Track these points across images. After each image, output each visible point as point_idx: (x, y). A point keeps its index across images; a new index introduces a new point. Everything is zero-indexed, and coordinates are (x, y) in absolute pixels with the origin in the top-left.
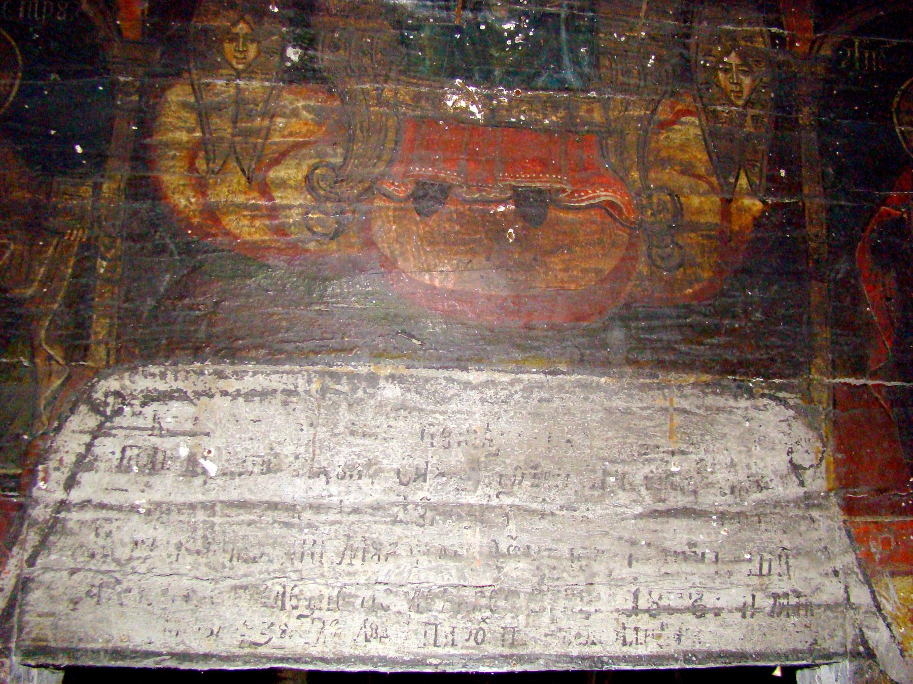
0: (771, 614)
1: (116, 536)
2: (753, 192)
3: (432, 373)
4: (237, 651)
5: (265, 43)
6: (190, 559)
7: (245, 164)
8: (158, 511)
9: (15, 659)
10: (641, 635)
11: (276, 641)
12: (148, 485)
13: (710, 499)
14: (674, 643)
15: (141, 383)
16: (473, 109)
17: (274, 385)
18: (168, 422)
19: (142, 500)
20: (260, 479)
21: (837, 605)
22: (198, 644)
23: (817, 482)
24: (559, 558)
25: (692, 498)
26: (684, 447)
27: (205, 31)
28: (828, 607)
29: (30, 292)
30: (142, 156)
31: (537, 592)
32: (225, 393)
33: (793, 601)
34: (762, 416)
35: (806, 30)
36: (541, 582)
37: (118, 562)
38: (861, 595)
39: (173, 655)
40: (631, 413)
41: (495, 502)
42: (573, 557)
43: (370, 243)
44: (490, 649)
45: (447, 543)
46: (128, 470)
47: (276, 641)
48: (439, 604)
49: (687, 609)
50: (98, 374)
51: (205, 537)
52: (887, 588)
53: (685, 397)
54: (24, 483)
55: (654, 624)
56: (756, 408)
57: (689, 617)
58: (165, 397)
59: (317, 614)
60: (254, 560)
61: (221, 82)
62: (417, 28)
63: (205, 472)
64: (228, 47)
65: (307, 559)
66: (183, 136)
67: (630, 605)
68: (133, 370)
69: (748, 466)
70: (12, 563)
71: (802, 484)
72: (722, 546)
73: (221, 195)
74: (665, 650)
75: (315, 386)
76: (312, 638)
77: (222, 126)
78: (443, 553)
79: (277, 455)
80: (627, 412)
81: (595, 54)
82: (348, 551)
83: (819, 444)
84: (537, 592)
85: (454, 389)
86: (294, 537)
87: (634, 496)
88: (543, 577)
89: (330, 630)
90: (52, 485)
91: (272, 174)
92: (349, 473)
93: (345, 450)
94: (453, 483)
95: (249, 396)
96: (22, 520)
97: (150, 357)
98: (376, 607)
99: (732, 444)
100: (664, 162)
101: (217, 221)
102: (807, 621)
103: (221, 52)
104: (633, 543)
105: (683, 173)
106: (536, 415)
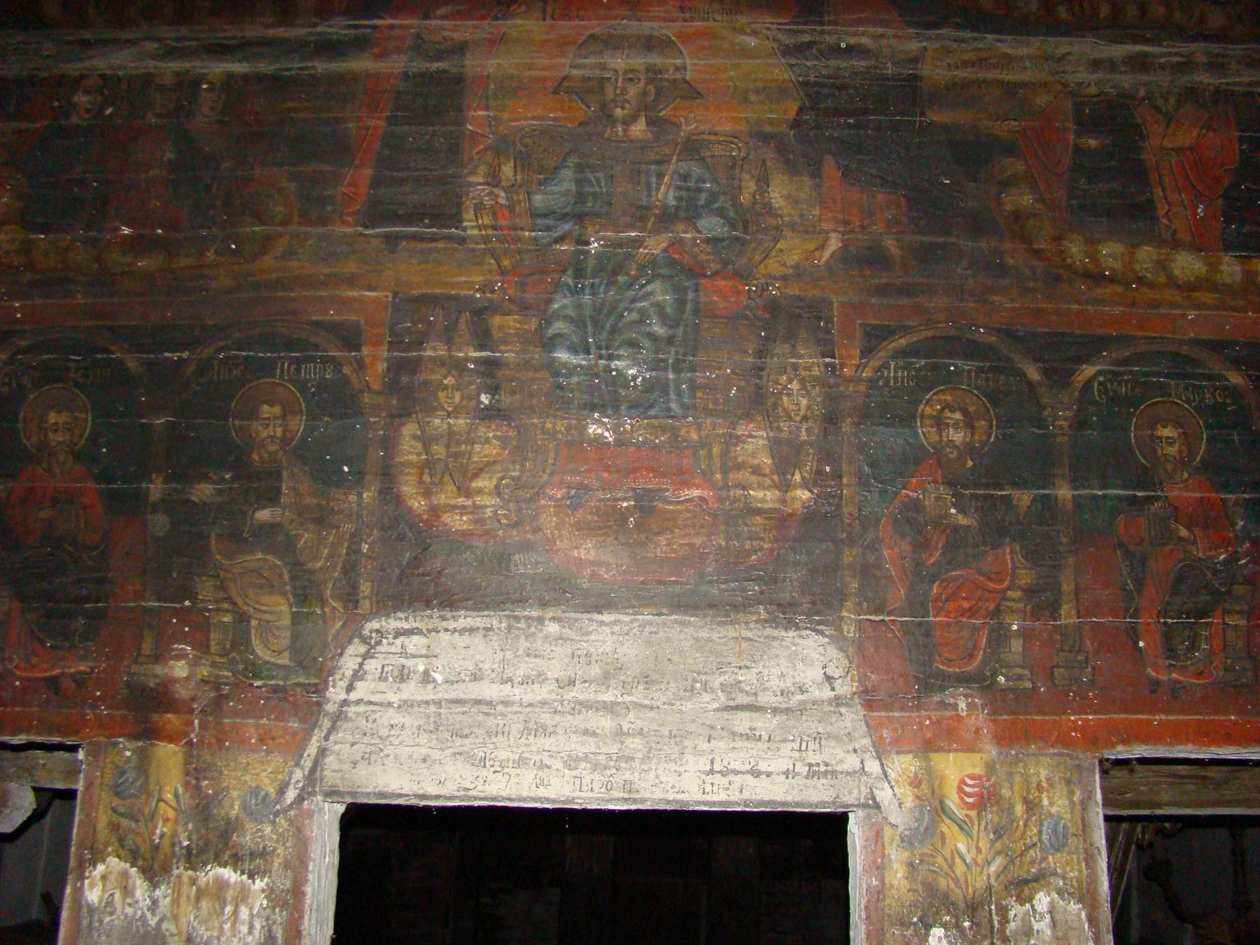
0: (807, 777)
1: (379, 721)
2: (805, 485)
3: (579, 615)
4: (457, 794)
5: (465, 391)
6: (426, 736)
7: (456, 477)
8: (405, 705)
9: (320, 798)
10: (715, 788)
11: (480, 787)
12: (398, 689)
13: (765, 699)
14: (737, 794)
15: (393, 624)
16: (607, 434)
17: (478, 624)
18: (411, 649)
19: (395, 699)
20: (471, 685)
21: (855, 772)
22: (433, 790)
23: (845, 688)
24: (662, 737)
25: (753, 698)
26: (748, 664)
27: (426, 383)
28: (848, 773)
29: (319, 565)
30: (388, 475)
31: (646, 758)
32: (446, 630)
33: (823, 768)
34: (804, 642)
35: (851, 357)
36: (649, 752)
37: (381, 738)
38: (873, 766)
39: (416, 796)
40: (712, 641)
41: (620, 699)
42: (671, 736)
43: (537, 530)
44: (615, 794)
45: (588, 726)
46: (386, 680)
47: (480, 787)
48: (583, 765)
49: (748, 772)
50: (367, 618)
51: (435, 722)
52: (893, 762)
53: (751, 630)
54: (319, 689)
55: (725, 781)
56: (801, 637)
57: (749, 777)
58: (408, 633)
59: (506, 770)
60: (466, 736)
61: (437, 421)
62: (569, 375)
63: (435, 681)
64: (442, 395)
65: (500, 735)
66: (414, 458)
67: (708, 768)
68: (388, 616)
69: (793, 677)
70: (314, 739)
71: (833, 689)
72: (774, 730)
73: (441, 499)
74: (732, 798)
75: (504, 625)
76: (502, 786)
77: (439, 450)
78: (586, 732)
79: (480, 670)
80: (709, 640)
81: (694, 387)
82: (526, 731)
83: (847, 662)
84: (646, 758)
85: (594, 626)
86: (491, 722)
87: (713, 696)
88: (651, 748)
89: (513, 780)
90: (338, 689)
91: (474, 485)
92: (526, 681)
93: (523, 666)
94: (593, 687)
95: (462, 631)
96: (319, 712)
97: (397, 608)
98: (543, 766)
99: (783, 662)
100: (739, 467)
101: (439, 517)
102: (832, 782)
103: (436, 398)
104: (712, 727)
105: (753, 473)
106: (648, 643)
